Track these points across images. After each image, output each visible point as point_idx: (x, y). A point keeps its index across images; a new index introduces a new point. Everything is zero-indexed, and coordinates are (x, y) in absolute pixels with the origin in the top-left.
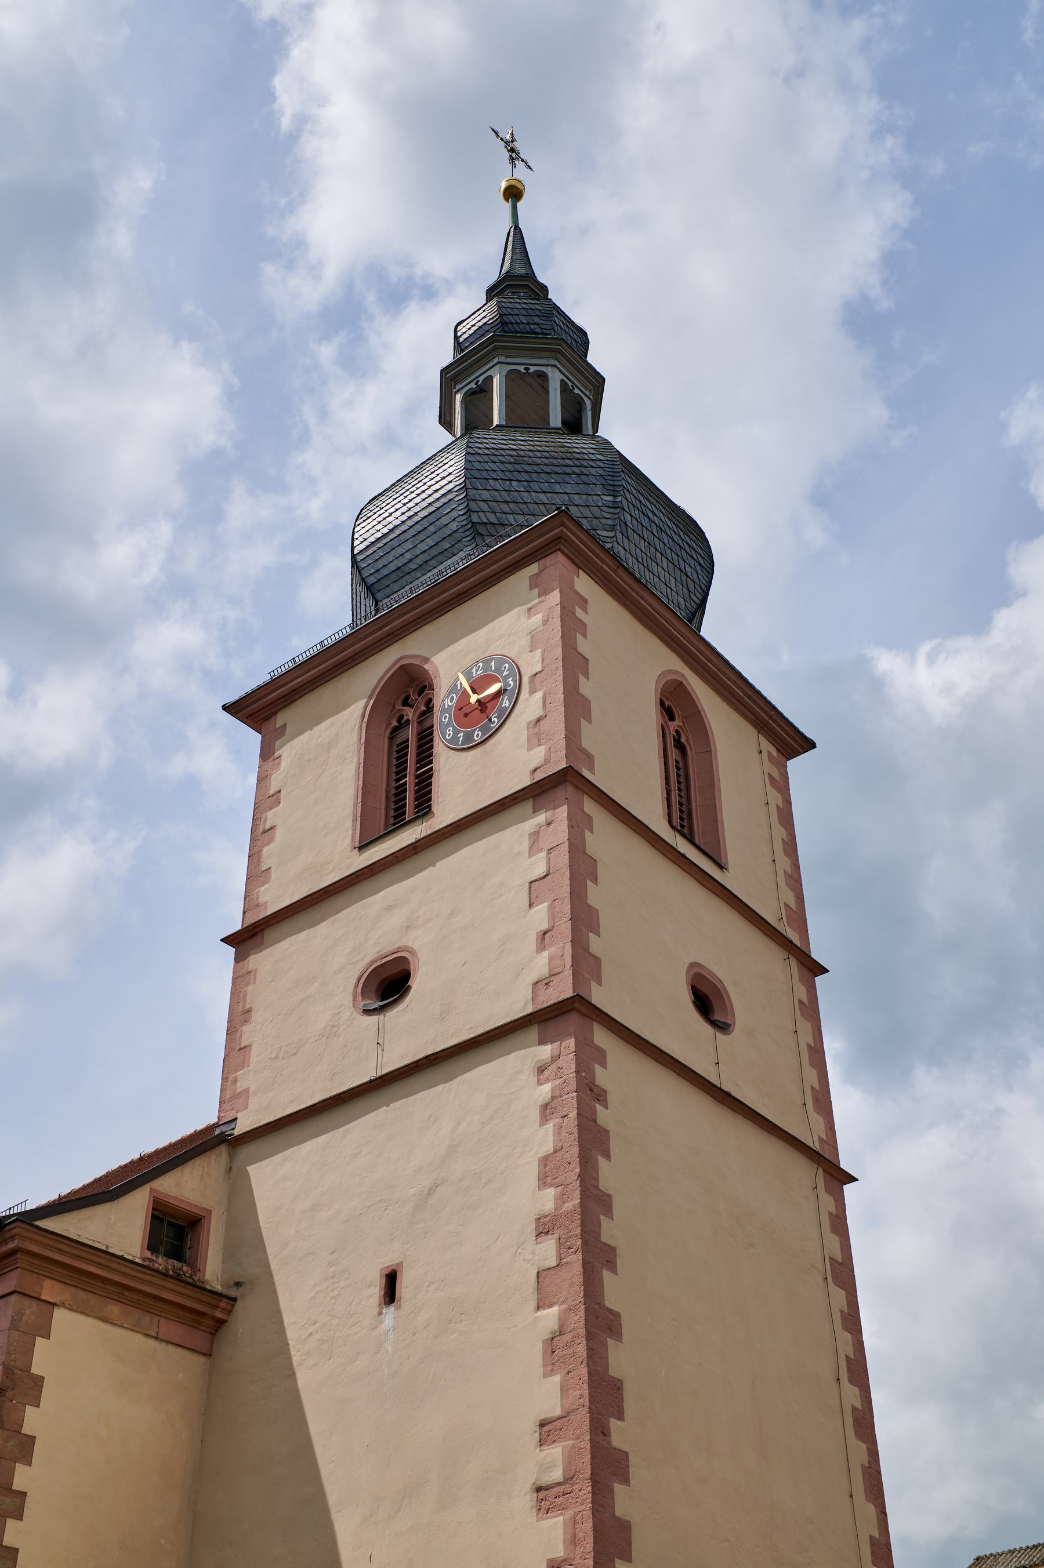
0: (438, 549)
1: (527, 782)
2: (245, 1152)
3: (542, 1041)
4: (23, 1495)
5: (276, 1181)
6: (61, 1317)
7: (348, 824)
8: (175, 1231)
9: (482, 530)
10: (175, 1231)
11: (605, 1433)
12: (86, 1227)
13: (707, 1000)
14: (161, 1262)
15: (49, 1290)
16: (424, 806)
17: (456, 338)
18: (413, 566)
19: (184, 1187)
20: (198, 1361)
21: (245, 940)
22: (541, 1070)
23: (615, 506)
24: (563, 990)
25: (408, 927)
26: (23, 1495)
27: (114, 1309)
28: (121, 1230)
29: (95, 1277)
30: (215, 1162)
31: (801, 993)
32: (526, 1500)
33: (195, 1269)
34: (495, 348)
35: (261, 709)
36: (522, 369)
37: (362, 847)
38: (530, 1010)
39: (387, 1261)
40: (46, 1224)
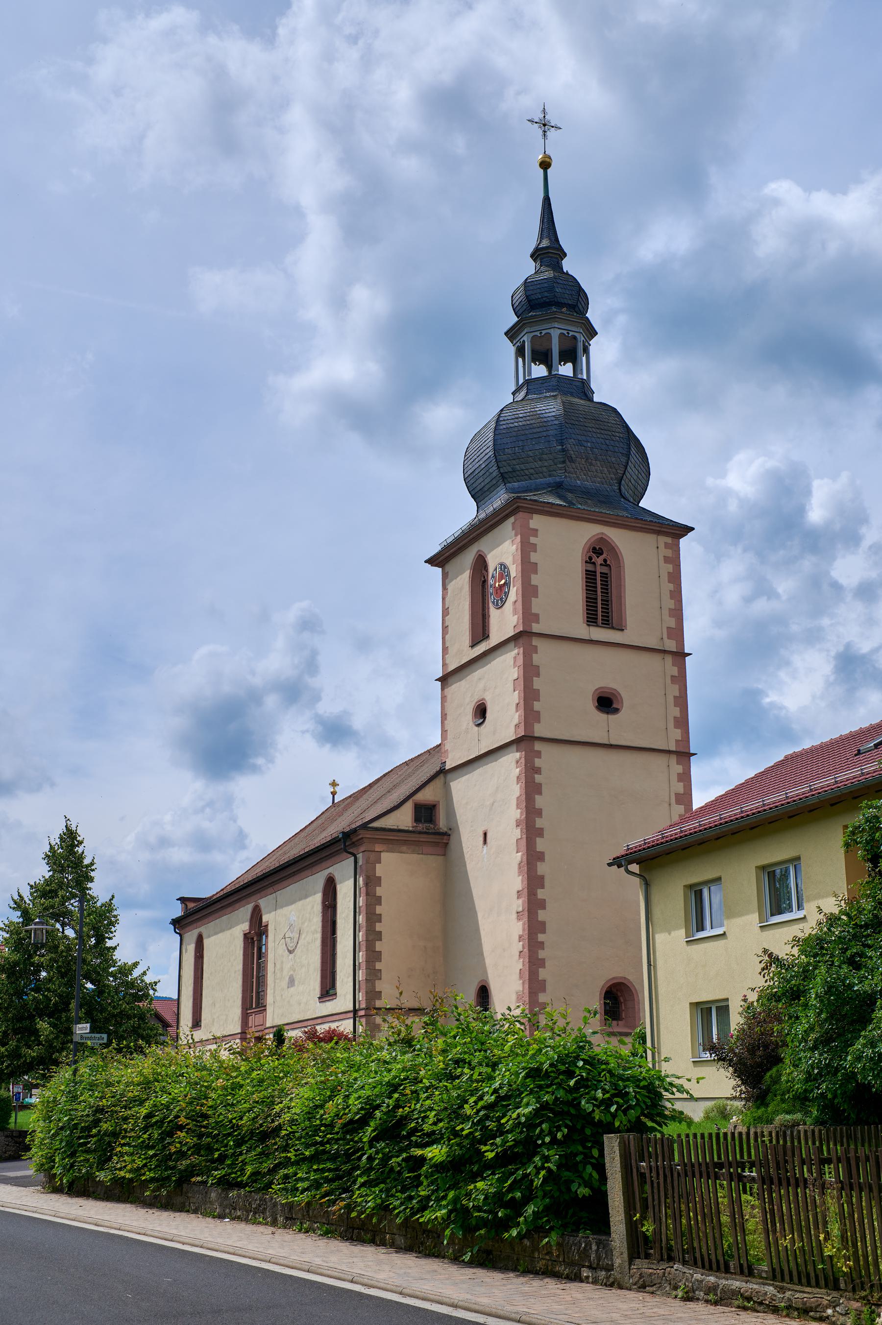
0: (491, 484)
1: (511, 633)
2: (449, 776)
3: (517, 751)
4: (380, 915)
5: (459, 787)
6: (384, 855)
7: (468, 633)
8: (425, 813)
9: (506, 476)
10: (425, 813)
11: (535, 894)
12: (388, 822)
13: (606, 703)
14: (421, 827)
15: (378, 848)
16: (485, 636)
17: (513, 306)
18: (486, 489)
19: (426, 796)
20: (440, 859)
21: (445, 680)
22: (517, 762)
23: (563, 450)
24: (521, 733)
25: (485, 690)
26: (380, 915)
27: (404, 848)
28: (404, 819)
29: (396, 839)
30: (438, 782)
31: (675, 671)
32: (515, 916)
33: (435, 825)
34: (524, 324)
35: (438, 560)
36: (538, 334)
37: (473, 646)
38: (514, 738)
39: (483, 829)
40: (375, 825)
